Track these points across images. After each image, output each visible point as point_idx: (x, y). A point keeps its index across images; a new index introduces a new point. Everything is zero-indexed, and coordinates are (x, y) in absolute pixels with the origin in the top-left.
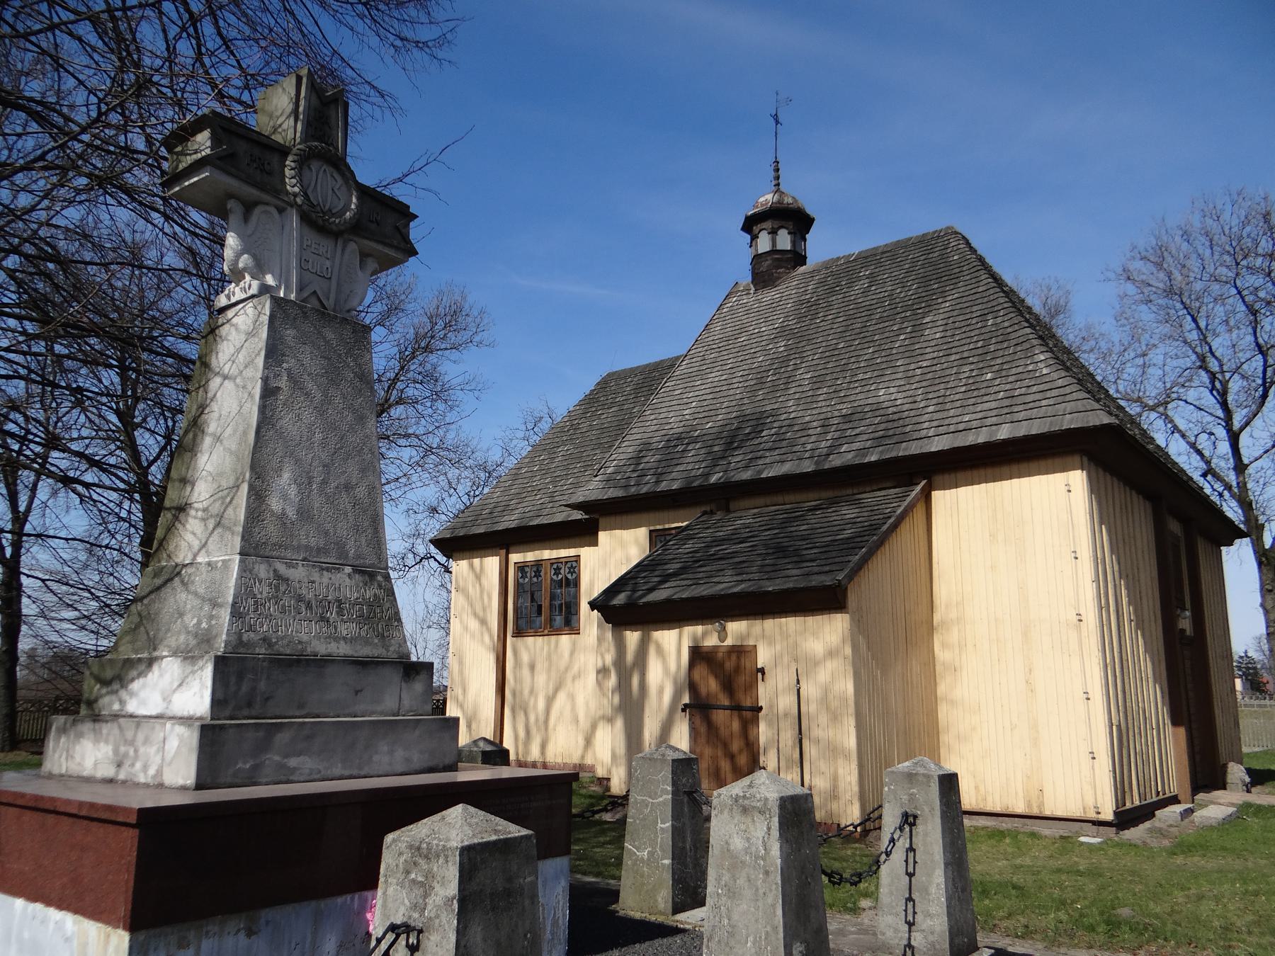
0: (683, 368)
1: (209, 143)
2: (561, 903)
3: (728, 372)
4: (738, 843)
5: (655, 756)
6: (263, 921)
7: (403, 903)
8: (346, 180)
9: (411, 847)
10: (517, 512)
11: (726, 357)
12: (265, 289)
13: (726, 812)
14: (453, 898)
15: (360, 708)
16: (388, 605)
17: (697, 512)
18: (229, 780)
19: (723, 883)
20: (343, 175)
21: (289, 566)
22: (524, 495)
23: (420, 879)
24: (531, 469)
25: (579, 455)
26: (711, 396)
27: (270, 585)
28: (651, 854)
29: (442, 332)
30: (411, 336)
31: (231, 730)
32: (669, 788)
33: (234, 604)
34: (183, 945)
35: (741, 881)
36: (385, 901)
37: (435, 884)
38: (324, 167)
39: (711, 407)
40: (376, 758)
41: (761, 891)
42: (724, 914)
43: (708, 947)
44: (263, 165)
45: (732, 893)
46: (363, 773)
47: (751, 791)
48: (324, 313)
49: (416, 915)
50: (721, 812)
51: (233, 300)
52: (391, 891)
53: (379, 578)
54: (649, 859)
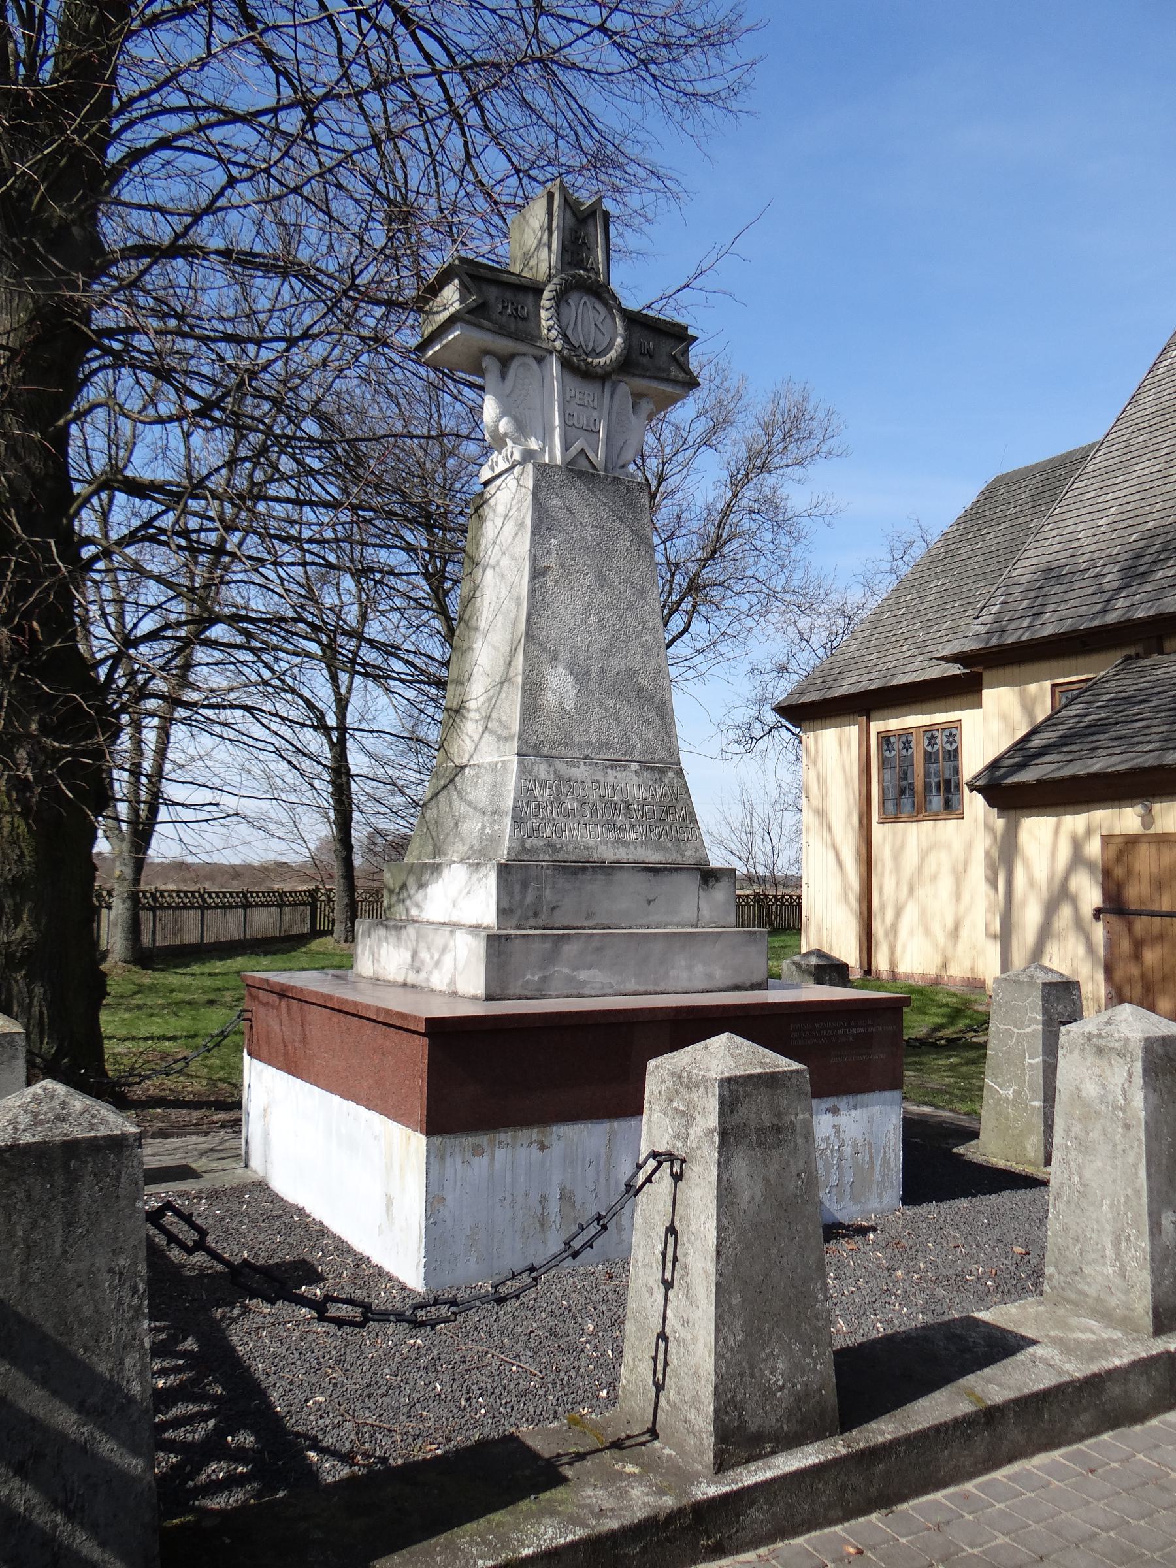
0: (1098, 462)
1: (457, 296)
2: (892, 1143)
3: (1163, 459)
4: (1091, 1090)
5: (1021, 978)
6: (554, 1136)
7: (666, 1131)
8: (609, 309)
9: (672, 1075)
10: (878, 668)
11: (1161, 439)
12: (528, 455)
13: (1076, 1052)
14: (714, 1130)
15: (655, 918)
16: (681, 804)
17: (1117, 657)
18: (518, 991)
19: (1073, 1134)
20: (605, 304)
21: (571, 765)
22: (887, 647)
23: (682, 1108)
24: (895, 613)
25: (957, 590)
26: (1137, 496)
27: (551, 787)
28: (1018, 1093)
29: (781, 446)
30: (744, 454)
31: (517, 941)
32: (1039, 1017)
33: (515, 808)
34: (477, 1151)
35: (1095, 1135)
36: (650, 1128)
37: (696, 1115)
38: (585, 298)
39: (1137, 512)
40: (672, 973)
41: (1120, 1148)
42: (1073, 1170)
43: (1055, 1206)
44: (516, 310)
45: (1084, 1147)
46: (658, 989)
47: (1109, 1028)
48: (592, 475)
49: (679, 1144)
50: (1071, 1052)
51: (497, 471)
52: (655, 1117)
53: (671, 774)
54: (1014, 1099)
